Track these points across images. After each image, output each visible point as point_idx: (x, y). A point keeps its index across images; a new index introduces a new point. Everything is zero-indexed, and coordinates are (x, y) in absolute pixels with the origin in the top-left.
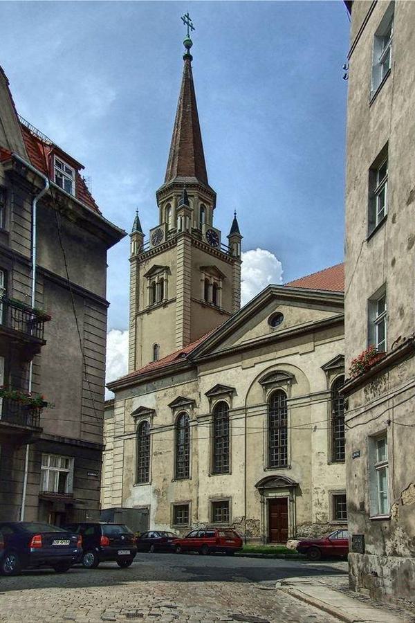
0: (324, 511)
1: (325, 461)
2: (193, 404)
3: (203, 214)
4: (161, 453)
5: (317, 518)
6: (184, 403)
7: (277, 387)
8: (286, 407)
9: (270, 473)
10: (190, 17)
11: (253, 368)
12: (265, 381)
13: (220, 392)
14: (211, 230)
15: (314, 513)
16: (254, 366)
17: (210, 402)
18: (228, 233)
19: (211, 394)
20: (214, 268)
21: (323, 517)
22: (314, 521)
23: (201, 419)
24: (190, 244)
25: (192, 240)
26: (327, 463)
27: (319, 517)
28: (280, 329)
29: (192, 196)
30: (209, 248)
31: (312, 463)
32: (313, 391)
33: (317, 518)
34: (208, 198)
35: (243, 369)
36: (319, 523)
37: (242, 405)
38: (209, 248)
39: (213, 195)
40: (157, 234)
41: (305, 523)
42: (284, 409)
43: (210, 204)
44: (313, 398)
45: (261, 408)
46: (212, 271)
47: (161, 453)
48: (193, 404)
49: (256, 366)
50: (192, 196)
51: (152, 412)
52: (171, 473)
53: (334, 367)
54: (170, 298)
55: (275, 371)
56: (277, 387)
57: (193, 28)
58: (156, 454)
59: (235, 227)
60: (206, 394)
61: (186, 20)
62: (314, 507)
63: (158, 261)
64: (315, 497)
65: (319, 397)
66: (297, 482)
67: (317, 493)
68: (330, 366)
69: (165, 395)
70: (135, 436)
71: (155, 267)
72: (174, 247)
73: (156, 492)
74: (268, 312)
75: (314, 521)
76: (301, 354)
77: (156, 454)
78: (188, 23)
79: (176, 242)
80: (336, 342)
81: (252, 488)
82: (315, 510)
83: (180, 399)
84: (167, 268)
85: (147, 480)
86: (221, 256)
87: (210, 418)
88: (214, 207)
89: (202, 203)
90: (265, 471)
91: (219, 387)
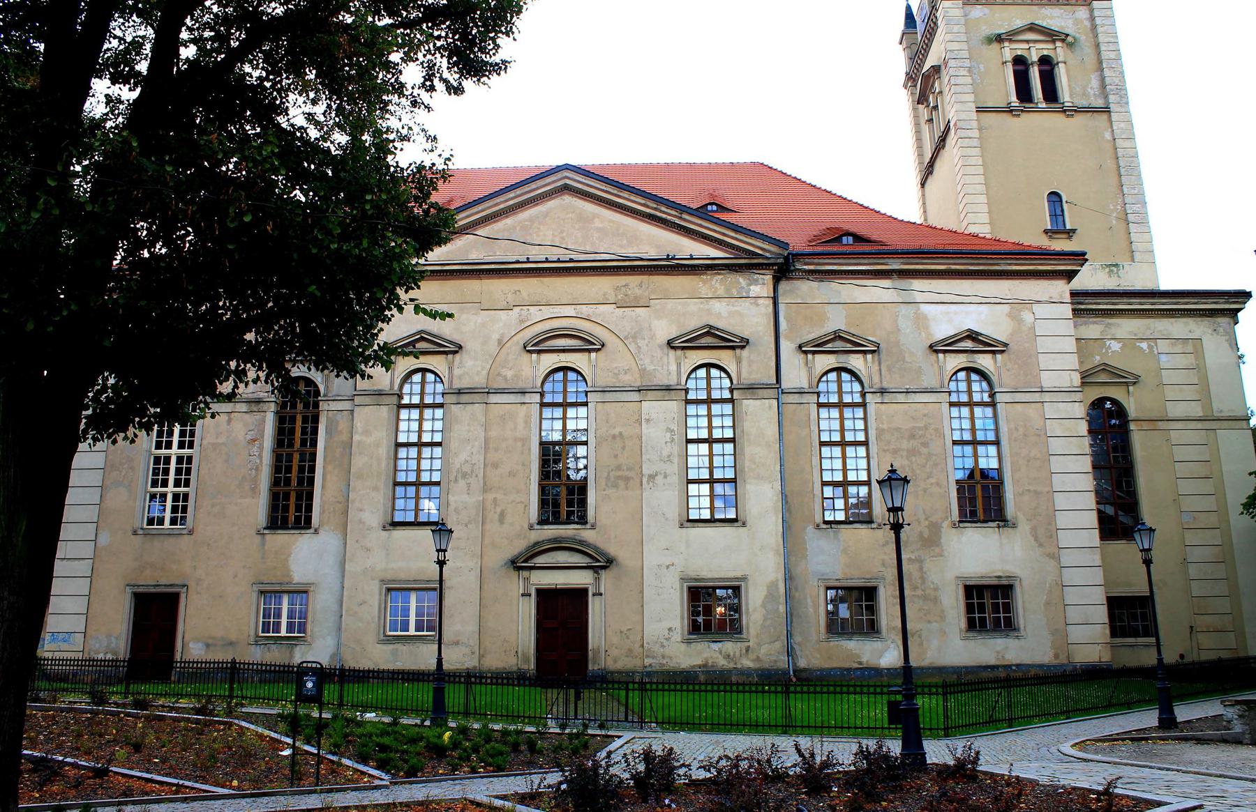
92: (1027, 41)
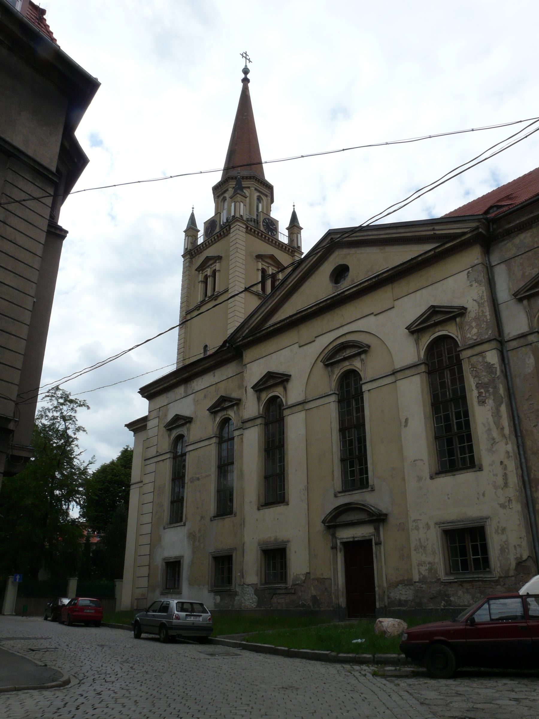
0: (430, 559)
1: (426, 473)
2: (237, 403)
3: (260, 205)
4: (198, 479)
5: (420, 573)
6: (227, 404)
7: (346, 366)
8: (362, 393)
9: (343, 500)
10: (247, 54)
11: (313, 344)
12: (327, 361)
13: (271, 382)
14: (269, 219)
15: (415, 562)
16: (314, 341)
17: (259, 399)
18: (287, 225)
19: (259, 388)
20: (272, 257)
21: (430, 570)
22: (416, 578)
23: (247, 425)
24: (244, 230)
25: (247, 227)
26: (428, 477)
27: (424, 570)
28: (345, 285)
29: (249, 188)
30: (265, 237)
31: (406, 478)
32: (398, 365)
33: (420, 573)
34: (266, 191)
35: (300, 347)
36: (423, 580)
37: (301, 398)
38: (265, 237)
39: (270, 188)
40: (211, 225)
41: (401, 582)
42: (359, 396)
43: (266, 196)
44: (399, 376)
45: (327, 400)
46: (269, 261)
47: (198, 479)
48: (237, 403)
49: (318, 339)
50: (249, 188)
51: (188, 420)
52: (212, 507)
53: (425, 325)
54: (222, 290)
55: (342, 343)
56: (346, 366)
57: (250, 61)
58: (192, 480)
59: (294, 218)
60: (253, 388)
61: (245, 55)
62: (413, 553)
63: (210, 252)
64: (414, 536)
65: (408, 373)
66: (384, 511)
67: (417, 528)
68: (416, 326)
69: (205, 397)
70: (168, 456)
71: (208, 259)
72: (227, 235)
73: (191, 536)
74: (328, 268)
75: (416, 578)
76: (375, 315)
77: (192, 480)
78: (246, 58)
79: (230, 229)
80: (424, 290)
81: (319, 527)
82: (416, 557)
83: (223, 399)
84: (219, 258)
85: (181, 520)
86: (280, 245)
87: (259, 421)
88: (272, 201)
89: (258, 194)
90: (336, 496)
91: (270, 375)
92: (268, 263)
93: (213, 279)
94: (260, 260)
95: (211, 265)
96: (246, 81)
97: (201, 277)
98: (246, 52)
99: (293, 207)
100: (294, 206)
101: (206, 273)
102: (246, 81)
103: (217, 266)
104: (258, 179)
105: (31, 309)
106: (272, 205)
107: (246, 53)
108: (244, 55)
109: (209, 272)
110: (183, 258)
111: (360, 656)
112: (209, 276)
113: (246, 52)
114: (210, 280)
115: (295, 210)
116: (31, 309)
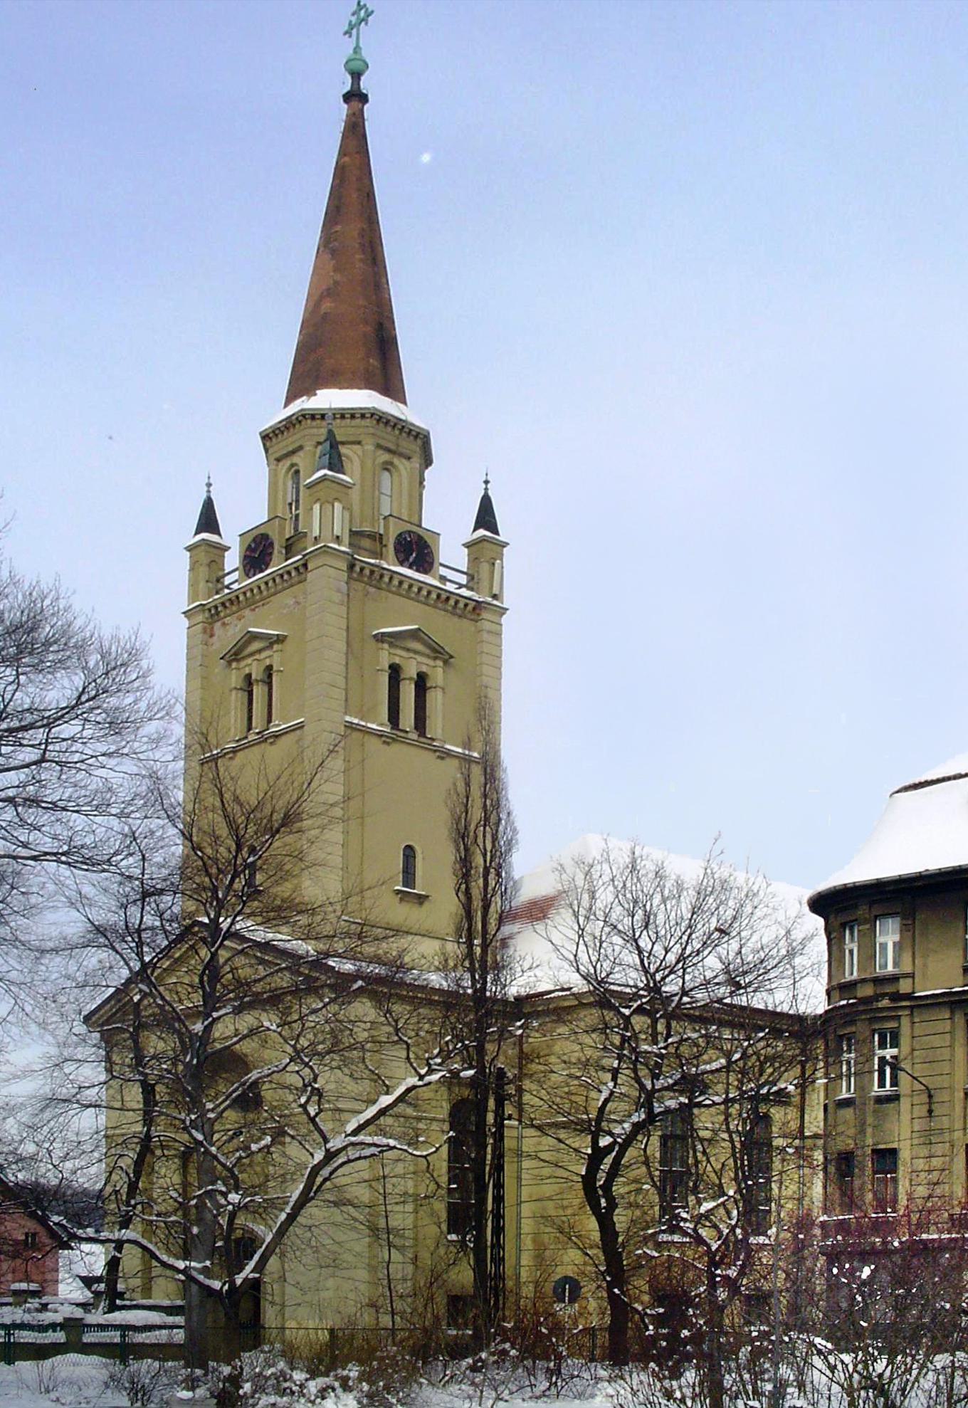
46: (417, 646)
88: (428, 461)
93: (266, 689)
94: (386, 646)
95: (260, 651)
96: (356, 97)
97: (235, 679)
98: (372, 12)
99: (484, 486)
100: (486, 482)
101: (247, 671)
102: (356, 97)
103: (275, 657)
104: (300, 418)
105: (389, 493)
106: (427, 473)
107: (369, 14)
108: (362, 13)
109: (257, 673)
110: (186, 620)
111: (868, 1135)
112: (257, 681)
113: (372, 12)
114: (259, 691)
115: (490, 493)
116: (389, 493)
